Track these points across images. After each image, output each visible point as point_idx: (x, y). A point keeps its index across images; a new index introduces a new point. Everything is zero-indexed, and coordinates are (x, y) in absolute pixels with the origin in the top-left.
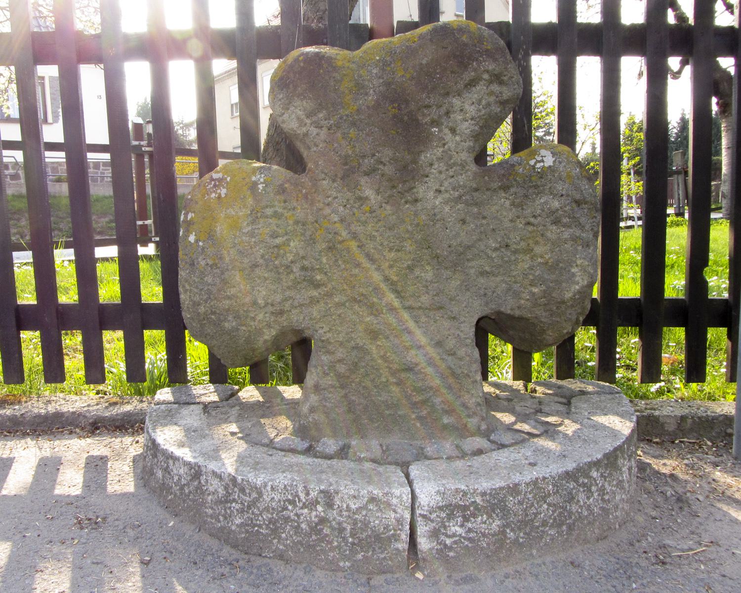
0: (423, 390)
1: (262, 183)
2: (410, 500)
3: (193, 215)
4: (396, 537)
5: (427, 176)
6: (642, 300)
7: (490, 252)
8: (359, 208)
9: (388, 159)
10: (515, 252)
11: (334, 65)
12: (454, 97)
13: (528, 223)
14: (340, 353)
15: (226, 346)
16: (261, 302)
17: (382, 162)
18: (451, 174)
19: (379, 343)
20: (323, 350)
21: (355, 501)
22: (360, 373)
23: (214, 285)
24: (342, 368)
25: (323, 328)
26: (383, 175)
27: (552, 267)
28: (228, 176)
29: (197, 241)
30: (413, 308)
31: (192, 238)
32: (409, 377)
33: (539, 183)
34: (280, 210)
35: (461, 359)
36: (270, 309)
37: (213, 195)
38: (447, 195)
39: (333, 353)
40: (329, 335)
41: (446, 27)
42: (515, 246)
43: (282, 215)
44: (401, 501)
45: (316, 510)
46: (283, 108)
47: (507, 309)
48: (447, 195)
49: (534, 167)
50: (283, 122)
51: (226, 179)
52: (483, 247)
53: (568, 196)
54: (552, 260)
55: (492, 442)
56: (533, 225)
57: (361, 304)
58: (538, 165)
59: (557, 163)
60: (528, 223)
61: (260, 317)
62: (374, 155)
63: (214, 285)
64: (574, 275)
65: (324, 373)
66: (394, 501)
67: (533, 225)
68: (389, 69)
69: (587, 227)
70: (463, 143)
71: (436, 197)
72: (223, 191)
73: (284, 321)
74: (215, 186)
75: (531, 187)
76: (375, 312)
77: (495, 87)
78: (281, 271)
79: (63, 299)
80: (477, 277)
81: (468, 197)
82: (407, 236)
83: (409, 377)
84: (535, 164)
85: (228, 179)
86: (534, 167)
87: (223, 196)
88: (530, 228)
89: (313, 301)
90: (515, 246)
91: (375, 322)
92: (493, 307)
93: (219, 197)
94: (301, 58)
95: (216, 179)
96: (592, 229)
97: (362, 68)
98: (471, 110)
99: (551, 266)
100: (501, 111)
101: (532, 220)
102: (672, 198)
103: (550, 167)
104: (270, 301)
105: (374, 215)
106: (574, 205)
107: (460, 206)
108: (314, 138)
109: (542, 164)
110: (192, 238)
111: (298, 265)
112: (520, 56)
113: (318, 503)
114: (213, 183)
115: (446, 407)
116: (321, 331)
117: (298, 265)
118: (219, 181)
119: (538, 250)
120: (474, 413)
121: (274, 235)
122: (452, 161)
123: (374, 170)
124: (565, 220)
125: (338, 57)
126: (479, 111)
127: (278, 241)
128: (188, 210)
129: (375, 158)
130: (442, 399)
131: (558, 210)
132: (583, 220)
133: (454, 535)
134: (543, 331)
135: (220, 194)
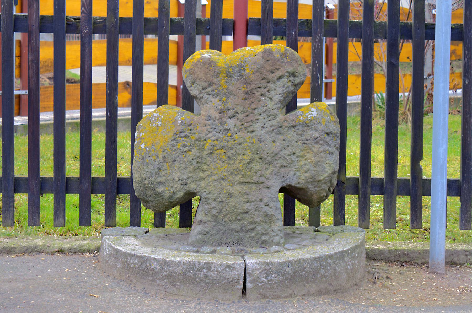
0: (253, 223)
1: (180, 120)
2: (244, 266)
3: (143, 134)
4: (238, 282)
5: (258, 120)
6: (461, 180)
7: (286, 156)
8: (226, 134)
9: (240, 111)
10: (298, 157)
11: (217, 66)
12: (272, 83)
13: (304, 143)
14: (214, 204)
15: (157, 201)
16: (177, 179)
17: (237, 113)
18: (269, 119)
19: (232, 199)
20: (206, 203)
21: (220, 267)
22: (223, 214)
23: (154, 170)
24: (214, 212)
25: (206, 192)
26: (238, 119)
27: (315, 165)
28: (162, 115)
29: (146, 148)
30: (249, 183)
31: (143, 146)
32: (246, 216)
33: (309, 125)
34: (188, 134)
35: (271, 208)
36: (180, 182)
37: (154, 124)
38: (267, 129)
39: (210, 204)
40: (209, 195)
41: (270, 51)
42: (297, 154)
43: (189, 136)
44: (240, 266)
45: (203, 272)
46: (191, 84)
47: (293, 184)
48: (267, 129)
49: (307, 117)
50: (191, 90)
51: (161, 116)
52: (283, 154)
53: (323, 131)
54: (315, 161)
55: (285, 248)
56: (306, 144)
57: (225, 180)
58: (310, 116)
59: (318, 115)
60: (304, 143)
61: (176, 186)
62: (234, 109)
63: (154, 170)
64: (325, 168)
65: (205, 214)
66: (238, 266)
67: (306, 144)
68: (242, 69)
69: (333, 145)
70: (275, 105)
71: (262, 130)
72: (160, 123)
73: (187, 188)
74: (155, 120)
75: (306, 126)
76: (231, 184)
77: (292, 78)
78: (187, 163)
79: (17, 174)
80: (280, 168)
81: (276, 130)
82: (248, 148)
83: (246, 216)
84: (308, 115)
85: (162, 117)
86: (307, 117)
87: (159, 125)
88: (305, 146)
89: (202, 179)
90: (297, 154)
91: (231, 189)
92: (287, 182)
93: (158, 125)
94: (201, 61)
95: (156, 116)
96: (335, 146)
97: (230, 68)
98: (280, 90)
99: (314, 164)
100: (294, 89)
101: (306, 142)
102: (452, 101)
103: (315, 117)
104: (181, 178)
105: (232, 137)
106: (325, 135)
107: (273, 134)
108: (206, 100)
109: (311, 115)
110: (143, 146)
111: (195, 161)
112: (317, 40)
113: (204, 268)
114: (154, 118)
115: (263, 232)
116: (205, 193)
117: (195, 161)
118: (157, 118)
119: (308, 156)
120: (277, 235)
121: (184, 146)
122: (270, 113)
123: (234, 116)
124: (322, 142)
125: (219, 61)
126: (284, 90)
127: (186, 149)
128: (140, 131)
129: (234, 110)
130: (262, 227)
131: (318, 137)
132: (330, 142)
133: (263, 282)
134: (312, 195)
135: (158, 125)
